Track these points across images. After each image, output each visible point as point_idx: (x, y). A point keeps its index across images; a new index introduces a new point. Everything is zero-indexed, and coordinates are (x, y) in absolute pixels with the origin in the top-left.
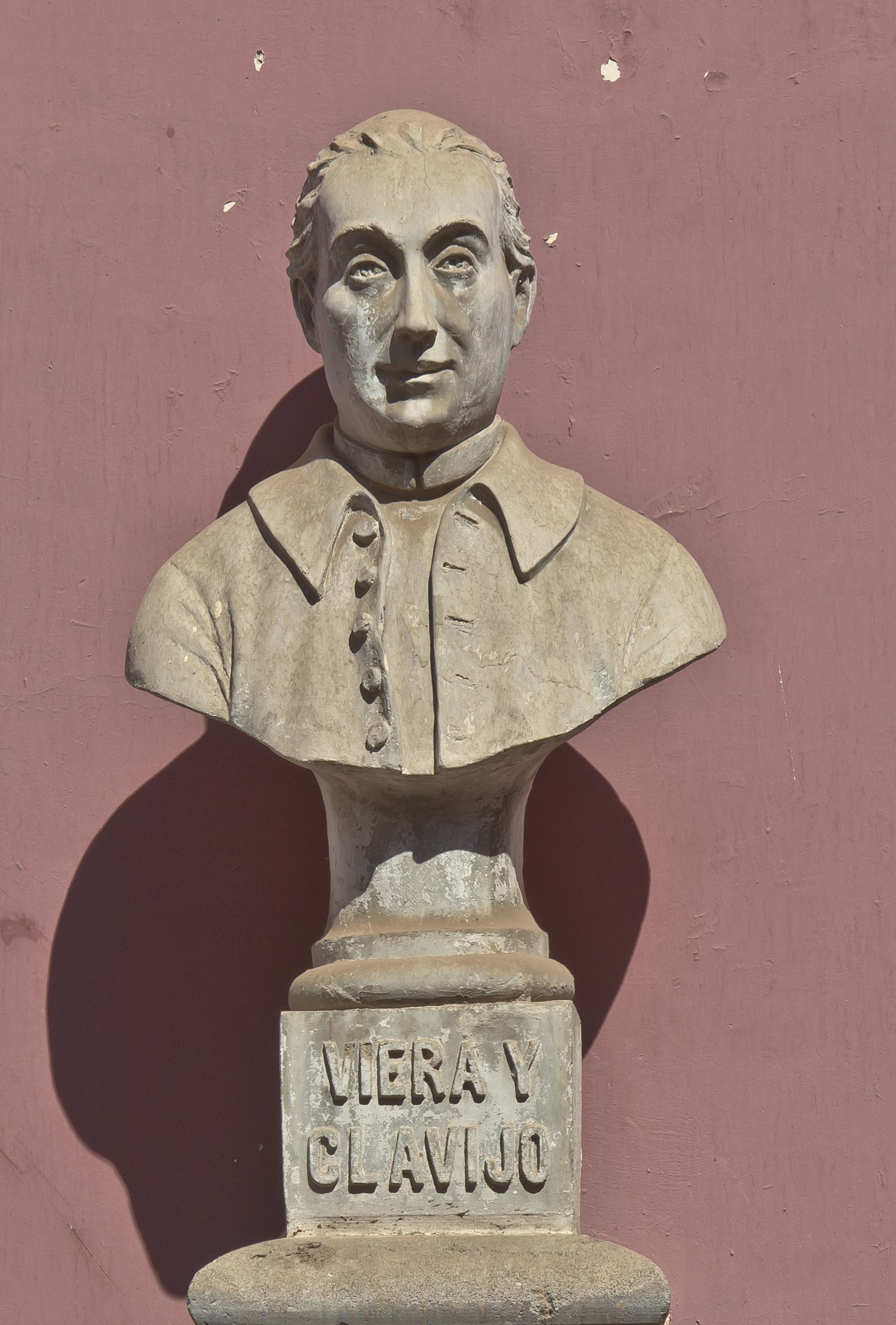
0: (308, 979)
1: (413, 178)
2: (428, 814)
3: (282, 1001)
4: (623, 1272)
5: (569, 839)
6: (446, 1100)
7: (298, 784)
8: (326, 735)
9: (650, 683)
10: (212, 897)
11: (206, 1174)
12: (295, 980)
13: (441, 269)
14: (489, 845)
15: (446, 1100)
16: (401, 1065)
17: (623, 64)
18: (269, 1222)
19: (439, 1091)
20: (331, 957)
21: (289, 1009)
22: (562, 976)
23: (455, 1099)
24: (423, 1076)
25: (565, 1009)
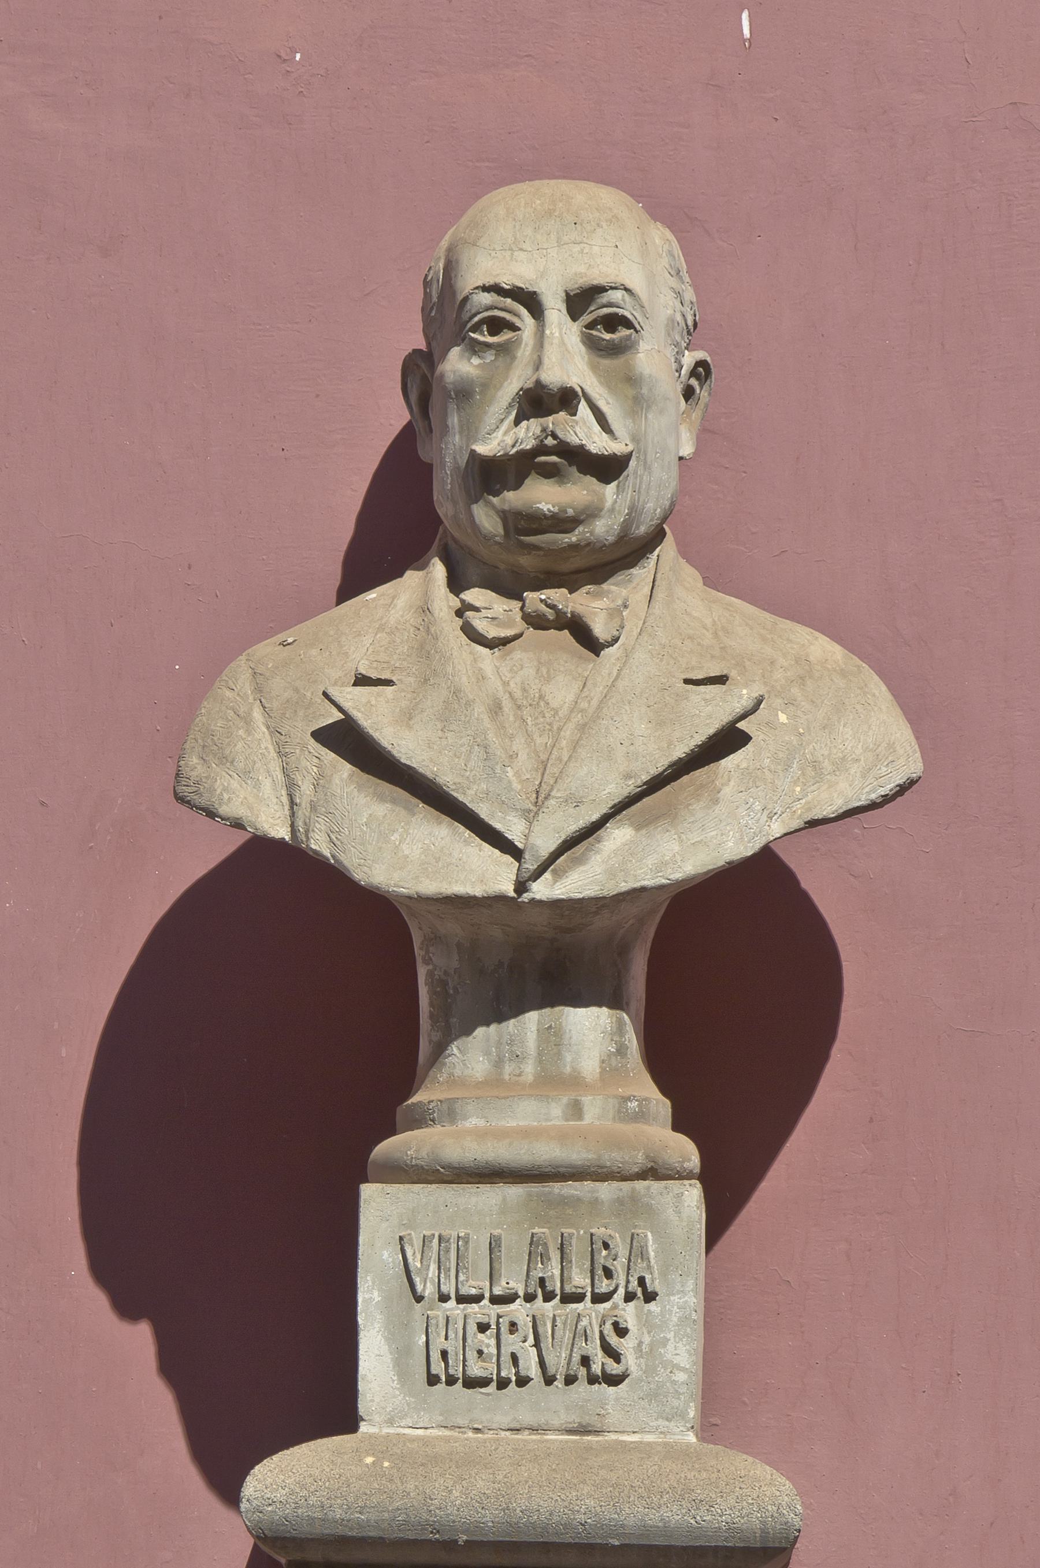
0: (386, 1148)
1: (542, 239)
2: (541, 959)
3: (358, 1171)
4: (750, 1492)
5: (735, 995)
6: (559, 1383)
8: (401, 855)
9: (812, 824)
10: (265, 1059)
11: (263, 1357)
12: (377, 1148)
13: (594, 332)
14: (615, 1001)
15: (559, 1383)
16: (487, 1341)
17: (368, 1455)
18: (339, 1413)
19: (551, 1371)
20: (420, 1119)
21: (368, 1182)
22: (685, 1151)
23: (570, 1380)
24: (518, 1257)
25: (693, 1195)
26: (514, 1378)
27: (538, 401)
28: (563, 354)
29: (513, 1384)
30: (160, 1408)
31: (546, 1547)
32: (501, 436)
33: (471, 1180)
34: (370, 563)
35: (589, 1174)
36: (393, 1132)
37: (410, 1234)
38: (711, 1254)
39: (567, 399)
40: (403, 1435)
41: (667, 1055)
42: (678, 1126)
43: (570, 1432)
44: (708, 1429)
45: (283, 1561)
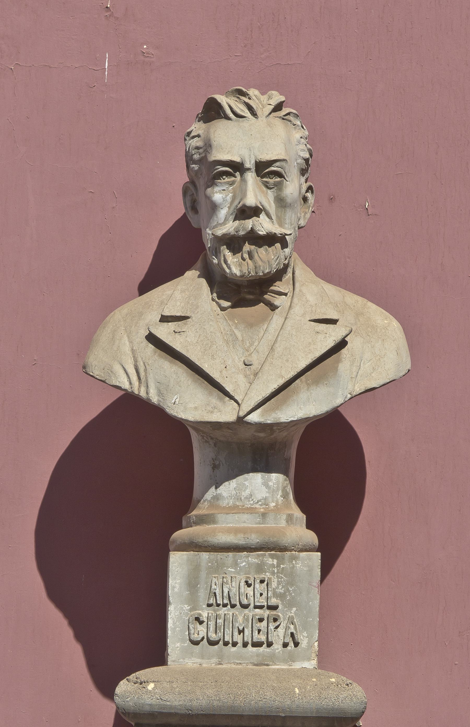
1: (254, 135)
2: (250, 448)
4: (341, 692)
5: (327, 469)
7: (179, 428)
10: (124, 494)
11: (118, 621)
14: (285, 473)
18: (158, 656)
22: (311, 537)
24: (239, 584)
26: (231, 642)
27: (246, 212)
28: (254, 192)
29: (230, 645)
30: (75, 654)
31: (257, 717)
32: (228, 226)
33: (195, 550)
34: (160, 273)
35: (263, 548)
36: (181, 528)
37: (236, 577)
38: (322, 585)
39: (255, 212)
40: (185, 670)
41: (305, 496)
42: (309, 526)
43: (255, 665)
44: (321, 664)
45: (133, 724)
